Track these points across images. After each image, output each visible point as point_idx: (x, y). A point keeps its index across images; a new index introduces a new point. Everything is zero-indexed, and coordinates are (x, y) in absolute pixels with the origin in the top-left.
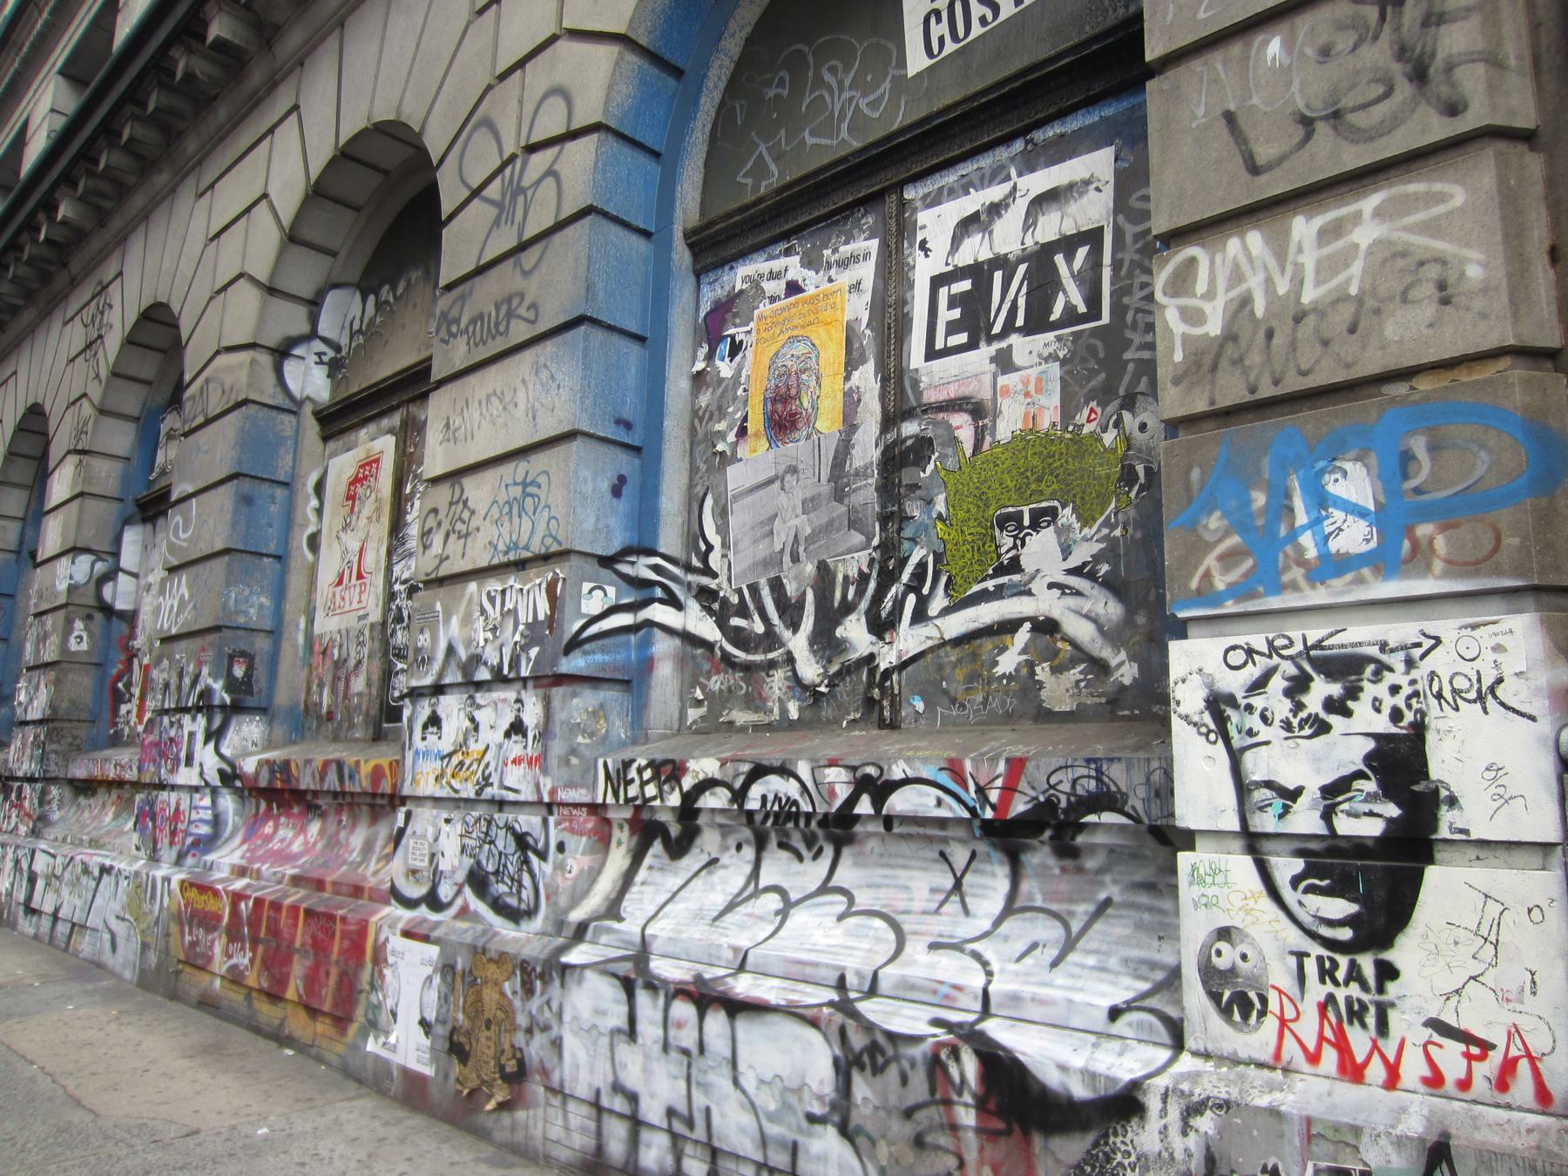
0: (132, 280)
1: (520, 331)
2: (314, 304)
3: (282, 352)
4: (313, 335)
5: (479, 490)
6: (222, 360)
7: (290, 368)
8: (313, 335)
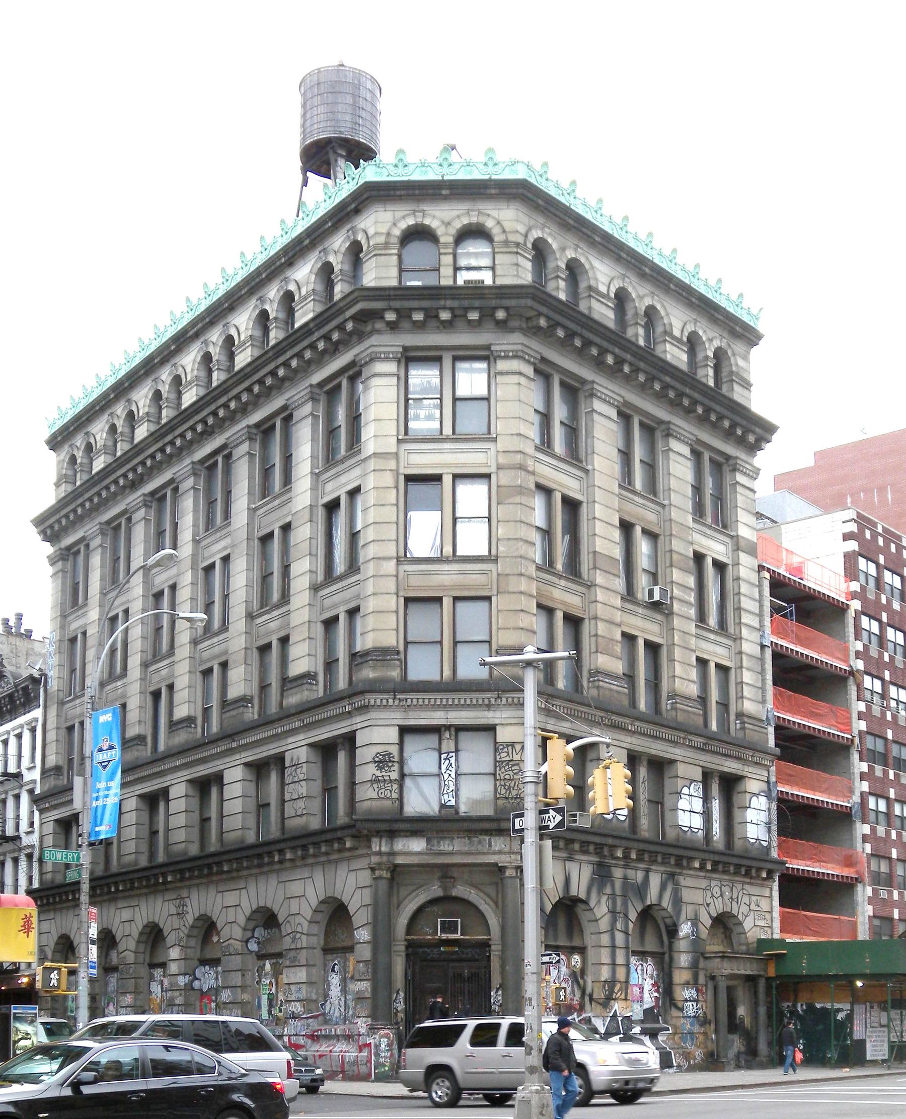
0: (195, 903)
1: (297, 964)
2: (253, 930)
3: (247, 942)
4: (253, 937)
5: (293, 987)
6: (231, 941)
7: (249, 945)
8: (253, 937)
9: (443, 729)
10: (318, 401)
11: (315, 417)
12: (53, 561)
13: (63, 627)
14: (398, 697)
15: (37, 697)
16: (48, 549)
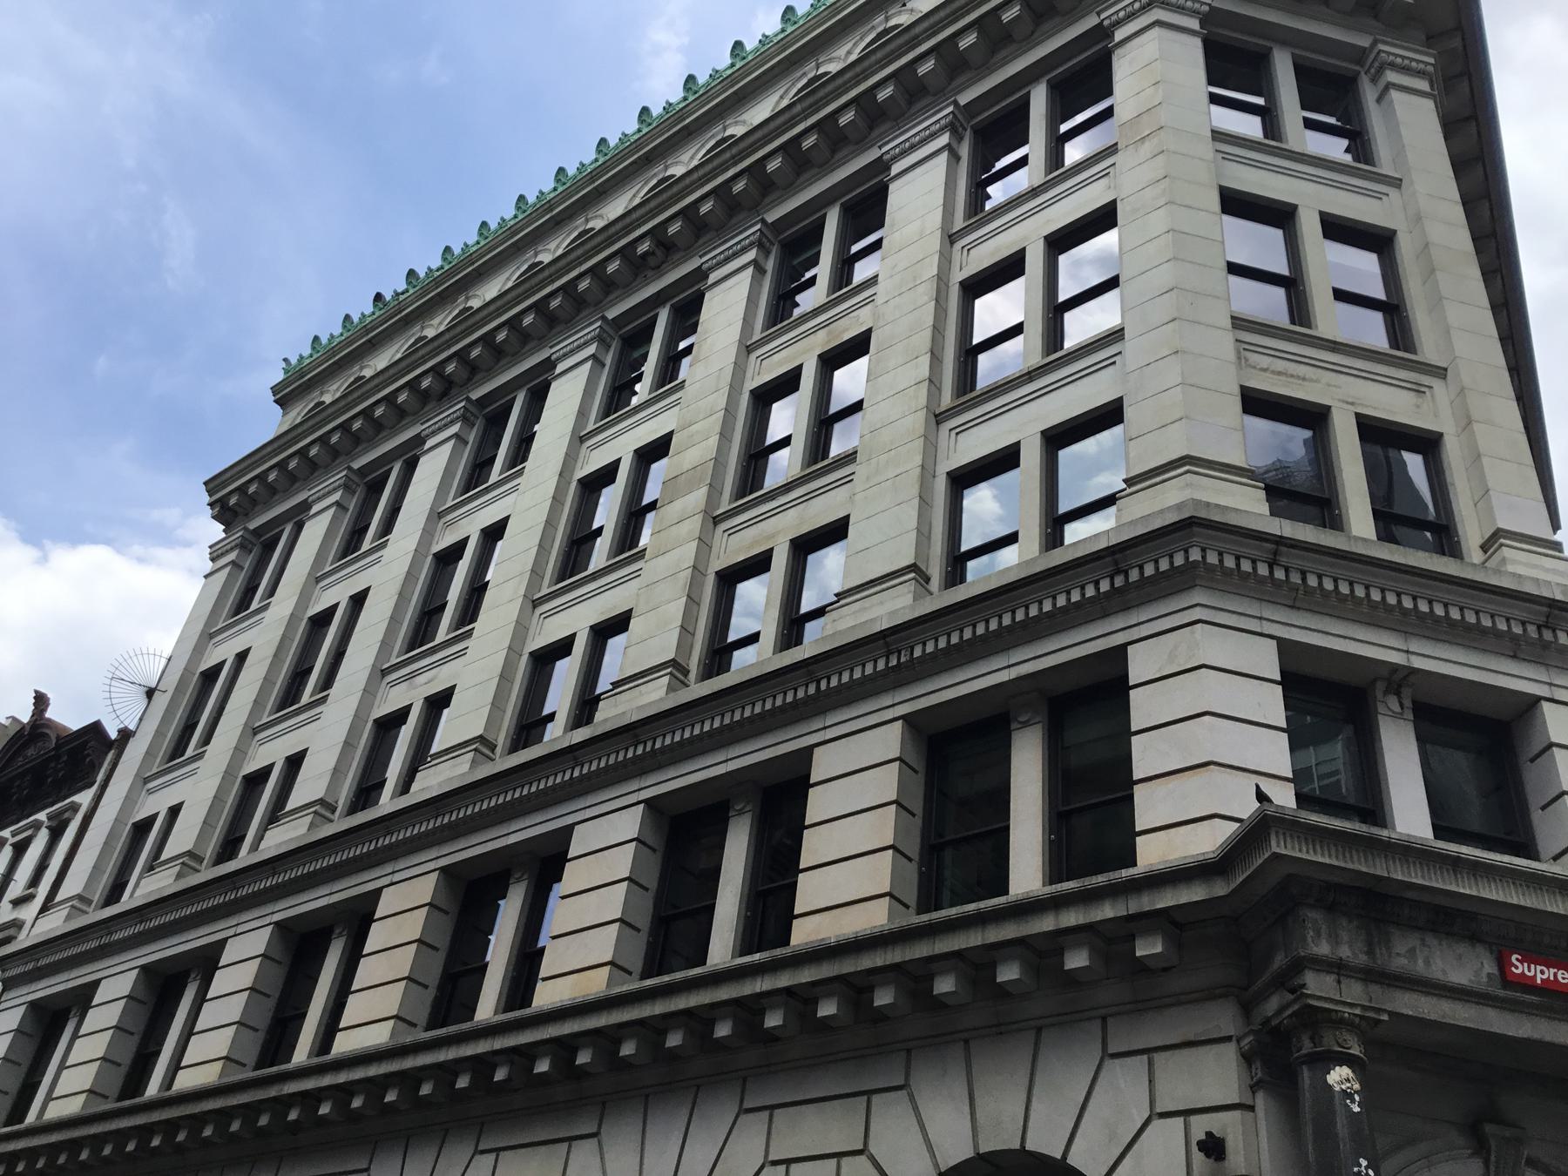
9: (1380, 687)
10: (354, 492)
11: (955, 157)
12: (211, 505)
13: (199, 650)
14: (1283, 560)
15: (95, 768)
16: (217, 531)
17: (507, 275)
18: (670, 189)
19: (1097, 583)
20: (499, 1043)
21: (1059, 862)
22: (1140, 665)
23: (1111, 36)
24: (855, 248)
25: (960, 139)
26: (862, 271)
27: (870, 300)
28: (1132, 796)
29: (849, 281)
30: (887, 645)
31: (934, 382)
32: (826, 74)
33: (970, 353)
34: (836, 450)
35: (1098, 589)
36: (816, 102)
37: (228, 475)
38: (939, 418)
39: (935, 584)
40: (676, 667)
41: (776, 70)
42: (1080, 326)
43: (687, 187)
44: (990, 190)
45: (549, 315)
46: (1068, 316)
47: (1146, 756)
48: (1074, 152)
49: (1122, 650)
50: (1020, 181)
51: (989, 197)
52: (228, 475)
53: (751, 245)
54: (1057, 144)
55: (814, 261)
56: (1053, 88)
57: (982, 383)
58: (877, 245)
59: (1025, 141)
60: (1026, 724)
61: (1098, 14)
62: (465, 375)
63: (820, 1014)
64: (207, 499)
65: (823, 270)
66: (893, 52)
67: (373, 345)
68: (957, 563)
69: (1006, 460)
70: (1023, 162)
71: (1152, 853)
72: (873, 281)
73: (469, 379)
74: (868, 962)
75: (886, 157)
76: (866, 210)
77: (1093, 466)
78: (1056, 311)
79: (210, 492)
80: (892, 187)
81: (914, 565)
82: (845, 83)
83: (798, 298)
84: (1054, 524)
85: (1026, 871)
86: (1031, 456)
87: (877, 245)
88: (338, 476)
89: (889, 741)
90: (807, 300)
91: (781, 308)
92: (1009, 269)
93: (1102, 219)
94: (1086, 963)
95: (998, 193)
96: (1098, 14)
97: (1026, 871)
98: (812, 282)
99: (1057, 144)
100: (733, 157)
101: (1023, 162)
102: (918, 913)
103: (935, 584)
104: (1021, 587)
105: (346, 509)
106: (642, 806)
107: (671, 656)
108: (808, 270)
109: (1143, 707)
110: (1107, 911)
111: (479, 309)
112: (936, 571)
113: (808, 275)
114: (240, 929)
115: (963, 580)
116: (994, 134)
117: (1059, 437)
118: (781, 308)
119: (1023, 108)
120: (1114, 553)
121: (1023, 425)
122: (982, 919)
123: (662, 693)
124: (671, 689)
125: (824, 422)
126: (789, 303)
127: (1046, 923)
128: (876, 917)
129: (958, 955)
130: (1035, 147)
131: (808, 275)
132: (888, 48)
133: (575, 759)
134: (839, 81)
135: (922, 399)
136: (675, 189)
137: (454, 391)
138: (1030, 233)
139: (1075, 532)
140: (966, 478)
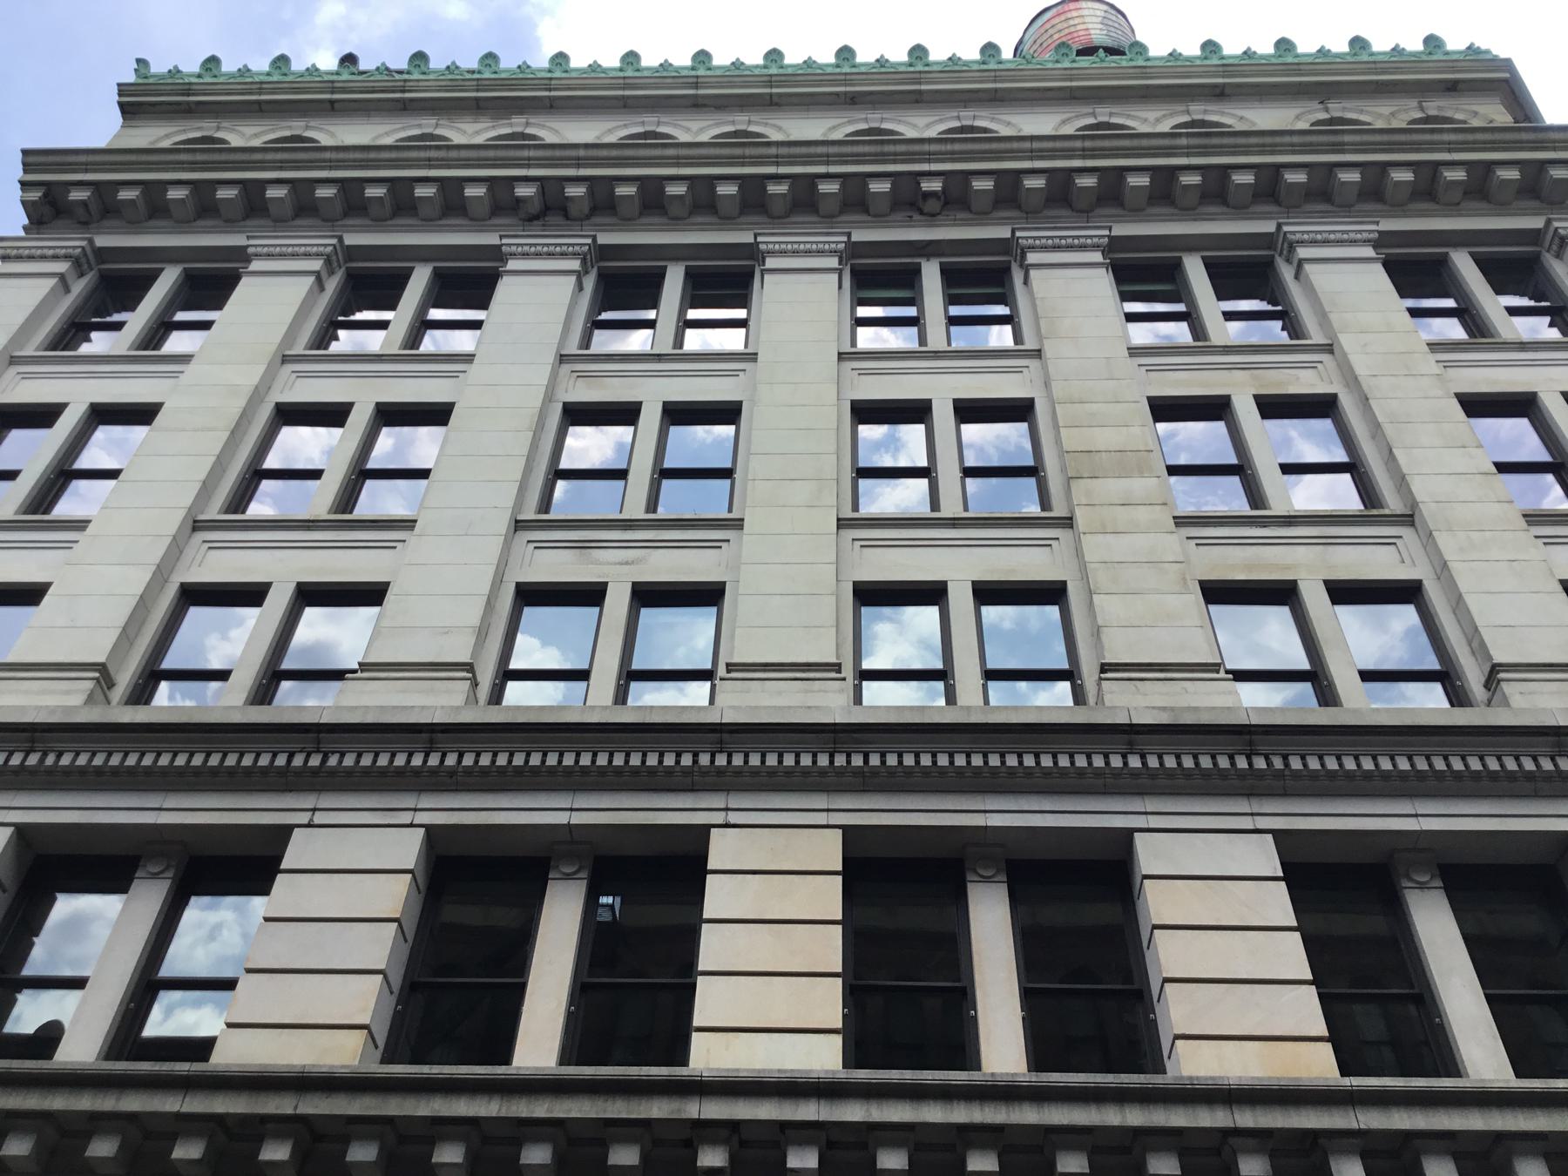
10: (82, 275)
17: (387, 128)
18: (879, 142)
19: (291, 756)
20: (541, 1109)
21: (582, 1039)
22: (722, 850)
23: (248, 261)
24: (181, 316)
25: (331, 273)
26: (177, 343)
27: (175, 375)
28: (694, 985)
29: (158, 346)
30: (431, 741)
31: (207, 489)
32: (534, 137)
33: (256, 475)
34: (65, 508)
35: (460, 761)
36: (1205, 147)
37: (83, 158)
38: (197, 526)
39: (118, 693)
40: (103, 674)
41: (1049, 94)
42: (378, 500)
43: (1012, 151)
44: (342, 333)
45: (800, 199)
46: (369, 483)
47: (713, 948)
48: (432, 342)
49: (705, 830)
50: (373, 341)
51: (337, 339)
52: (83, 158)
53: (66, 257)
54: (422, 325)
55: (131, 305)
56: (438, 275)
57: (363, 510)
58: (476, 325)
59: (392, 307)
60: (568, 877)
61: (501, 237)
62: (535, 207)
63: (261, 1157)
64: (18, 172)
65: (137, 320)
66: (1311, 144)
67: (697, 105)
68: (151, 677)
69: (251, 595)
70: (383, 325)
71: (708, 1055)
72: (185, 359)
73: (588, 217)
74: (1247, 1119)
75: (251, 250)
76: (209, 286)
77: (332, 634)
78: (361, 474)
79: (27, 167)
80: (244, 281)
81: (103, 665)
82: (1221, 146)
83: (94, 335)
84: (272, 677)
85: (538, 1043)
86: (278, 601)
87: (206, 325)
88: (326, 242)
89: (407, 849)
90: (99, 343)
91: (72, 333)
92: (333, 415)
93: (437, 414)
94: (459, 1160)
95: (346, 341)
96: (501, 237)
97: (538, 1043)
98: (118, 326)
99: (422, 325)
100: (1084, 149)
101: (383, 325)
102: (382, 1062)
103: (118, 693)
104: (475, 731)
105: (67, 290)
106: (12, 829)
107: (101, 659)
108: (119, 311)
109: (719, 897)
110: (933, 1114)
111: (325, 149)
112: (125, 678)
113: (116, 317)
114: (319, 818)
115: (148, 702)
116: (369, 285)
117: (312, 595)
118: (72, 333)
119: (148, 280)
120: (433, 731)
121: (280, 568)
122: (1122, 1097)
123: (77, 700)
124: (90, 700)
125: (63, 475)
126: (81, 334)
127: (85, 1102)
128: (344, 1053)
129: (734, 1126)
130: (400, 317)
131: (116, 317)
132: (970, 146)
133: (1130, 743)
134: (1002, 146)
135: (188, 500)
136: (216, 157)
137: (551, 219)
138: (364, 395)
139: (516, 693)
140: (532, 595)
